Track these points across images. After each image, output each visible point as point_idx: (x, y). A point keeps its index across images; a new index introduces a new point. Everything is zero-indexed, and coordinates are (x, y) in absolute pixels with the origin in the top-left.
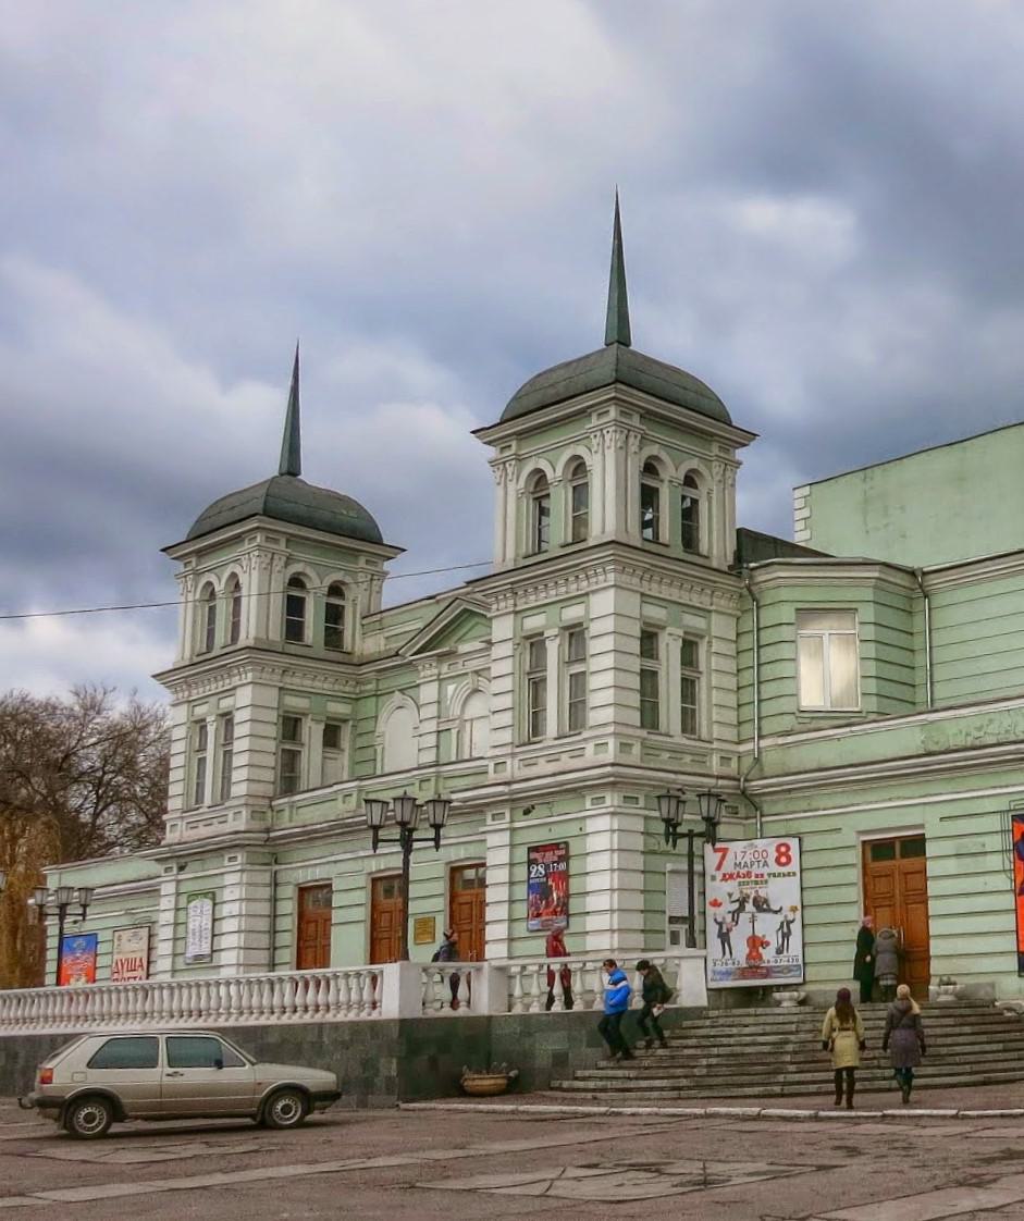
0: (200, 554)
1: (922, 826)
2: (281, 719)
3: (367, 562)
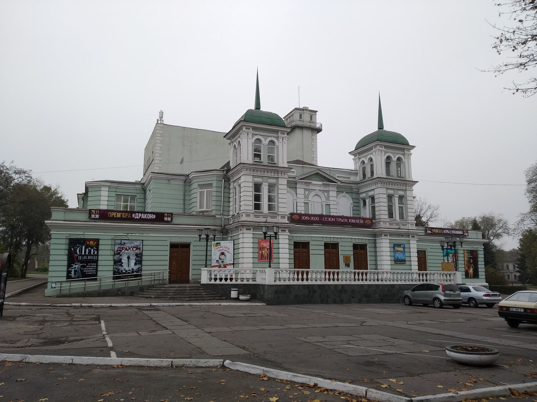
0: (360, 154)
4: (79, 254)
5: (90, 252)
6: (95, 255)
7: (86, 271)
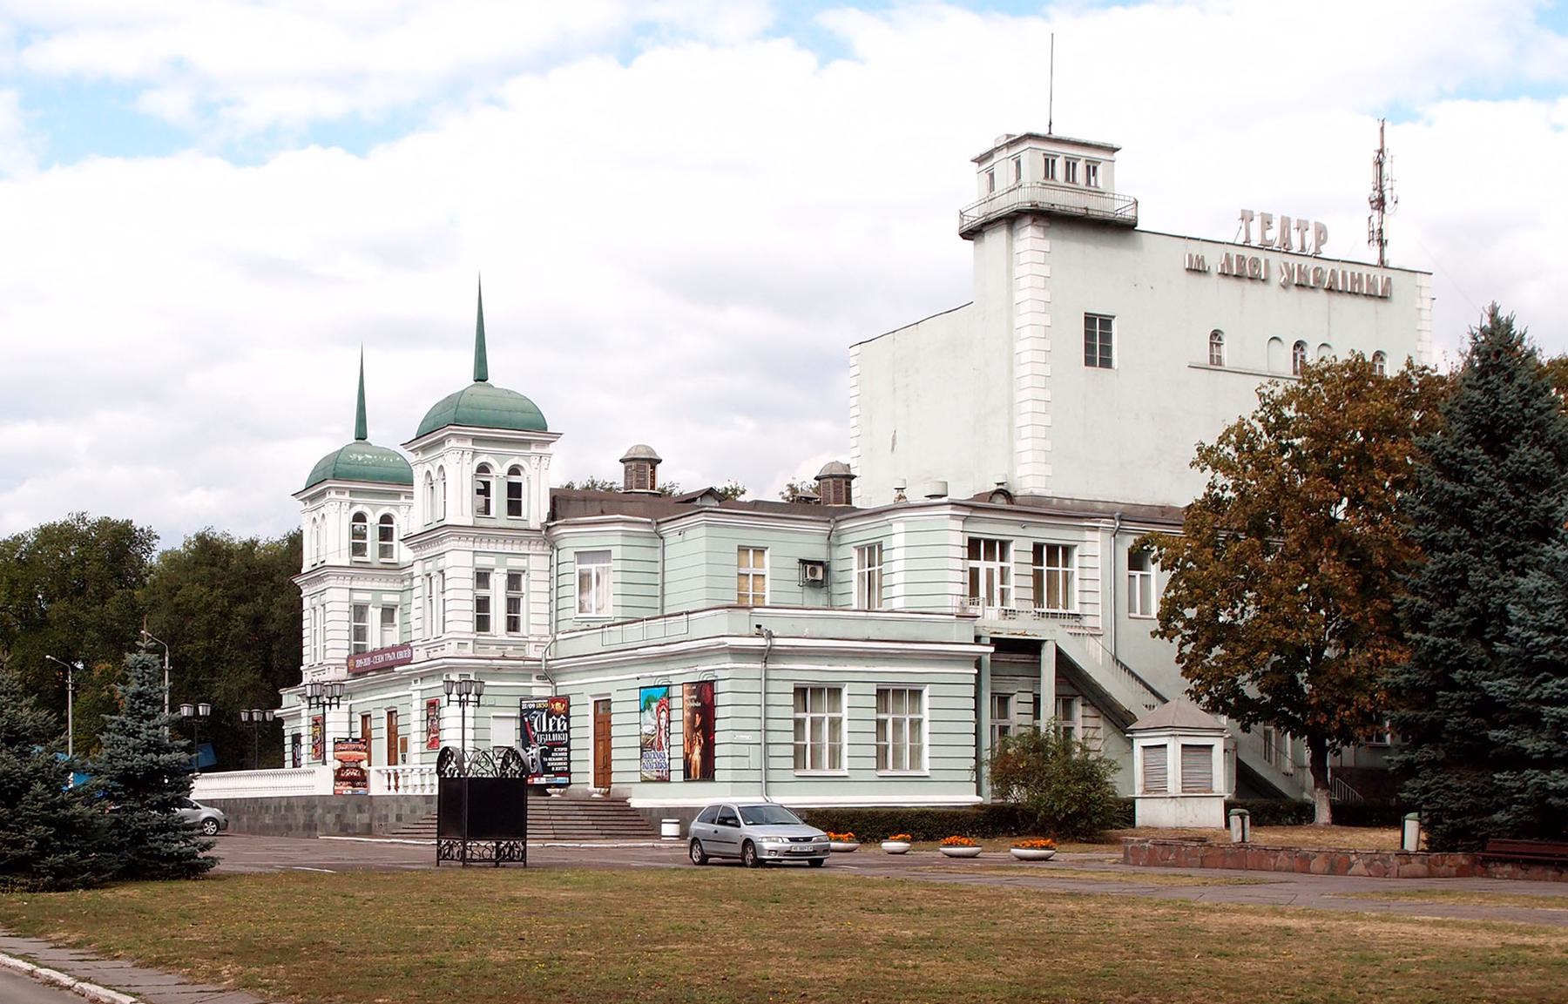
0: (312, 499)
1: (610, 694)
3: (406, 497)
5: (555, 726)
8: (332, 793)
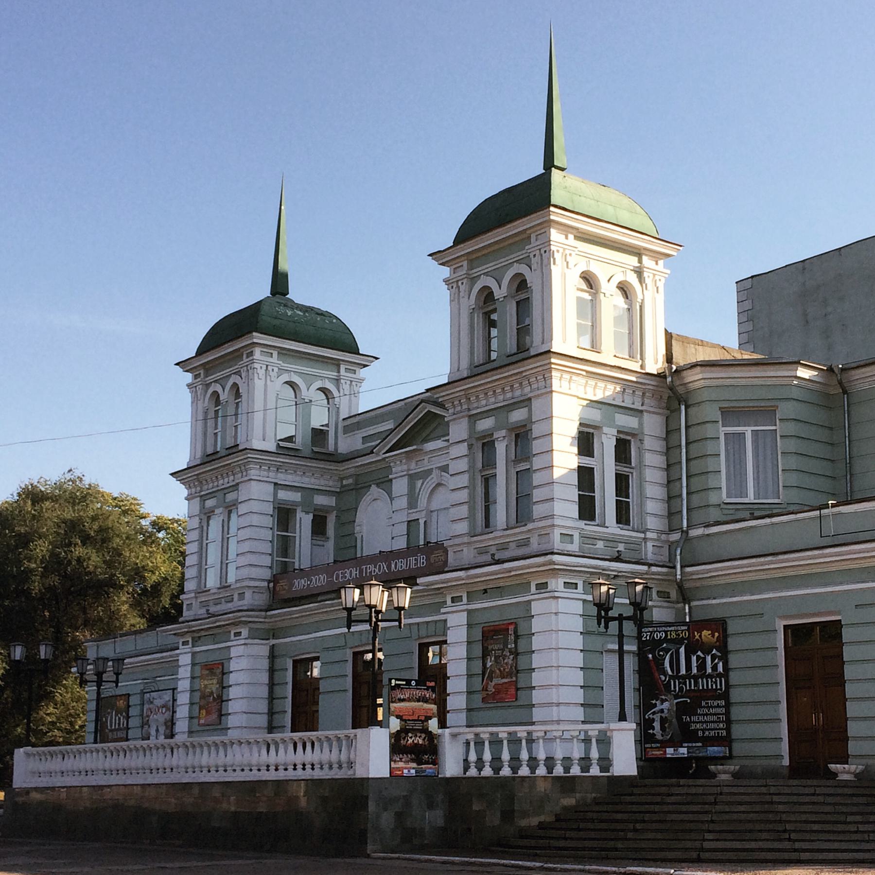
2: (276, 511)
4: (670, 673)
5: (702, 666)
6: (720, 675)
7: (698, 726)
8: (388, 776)
